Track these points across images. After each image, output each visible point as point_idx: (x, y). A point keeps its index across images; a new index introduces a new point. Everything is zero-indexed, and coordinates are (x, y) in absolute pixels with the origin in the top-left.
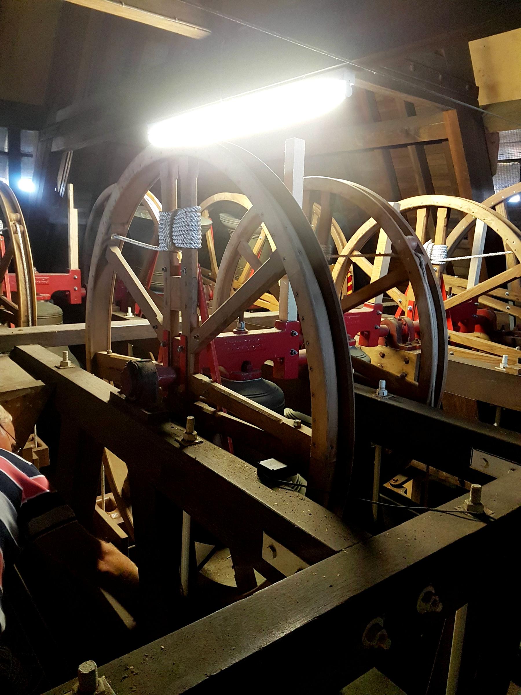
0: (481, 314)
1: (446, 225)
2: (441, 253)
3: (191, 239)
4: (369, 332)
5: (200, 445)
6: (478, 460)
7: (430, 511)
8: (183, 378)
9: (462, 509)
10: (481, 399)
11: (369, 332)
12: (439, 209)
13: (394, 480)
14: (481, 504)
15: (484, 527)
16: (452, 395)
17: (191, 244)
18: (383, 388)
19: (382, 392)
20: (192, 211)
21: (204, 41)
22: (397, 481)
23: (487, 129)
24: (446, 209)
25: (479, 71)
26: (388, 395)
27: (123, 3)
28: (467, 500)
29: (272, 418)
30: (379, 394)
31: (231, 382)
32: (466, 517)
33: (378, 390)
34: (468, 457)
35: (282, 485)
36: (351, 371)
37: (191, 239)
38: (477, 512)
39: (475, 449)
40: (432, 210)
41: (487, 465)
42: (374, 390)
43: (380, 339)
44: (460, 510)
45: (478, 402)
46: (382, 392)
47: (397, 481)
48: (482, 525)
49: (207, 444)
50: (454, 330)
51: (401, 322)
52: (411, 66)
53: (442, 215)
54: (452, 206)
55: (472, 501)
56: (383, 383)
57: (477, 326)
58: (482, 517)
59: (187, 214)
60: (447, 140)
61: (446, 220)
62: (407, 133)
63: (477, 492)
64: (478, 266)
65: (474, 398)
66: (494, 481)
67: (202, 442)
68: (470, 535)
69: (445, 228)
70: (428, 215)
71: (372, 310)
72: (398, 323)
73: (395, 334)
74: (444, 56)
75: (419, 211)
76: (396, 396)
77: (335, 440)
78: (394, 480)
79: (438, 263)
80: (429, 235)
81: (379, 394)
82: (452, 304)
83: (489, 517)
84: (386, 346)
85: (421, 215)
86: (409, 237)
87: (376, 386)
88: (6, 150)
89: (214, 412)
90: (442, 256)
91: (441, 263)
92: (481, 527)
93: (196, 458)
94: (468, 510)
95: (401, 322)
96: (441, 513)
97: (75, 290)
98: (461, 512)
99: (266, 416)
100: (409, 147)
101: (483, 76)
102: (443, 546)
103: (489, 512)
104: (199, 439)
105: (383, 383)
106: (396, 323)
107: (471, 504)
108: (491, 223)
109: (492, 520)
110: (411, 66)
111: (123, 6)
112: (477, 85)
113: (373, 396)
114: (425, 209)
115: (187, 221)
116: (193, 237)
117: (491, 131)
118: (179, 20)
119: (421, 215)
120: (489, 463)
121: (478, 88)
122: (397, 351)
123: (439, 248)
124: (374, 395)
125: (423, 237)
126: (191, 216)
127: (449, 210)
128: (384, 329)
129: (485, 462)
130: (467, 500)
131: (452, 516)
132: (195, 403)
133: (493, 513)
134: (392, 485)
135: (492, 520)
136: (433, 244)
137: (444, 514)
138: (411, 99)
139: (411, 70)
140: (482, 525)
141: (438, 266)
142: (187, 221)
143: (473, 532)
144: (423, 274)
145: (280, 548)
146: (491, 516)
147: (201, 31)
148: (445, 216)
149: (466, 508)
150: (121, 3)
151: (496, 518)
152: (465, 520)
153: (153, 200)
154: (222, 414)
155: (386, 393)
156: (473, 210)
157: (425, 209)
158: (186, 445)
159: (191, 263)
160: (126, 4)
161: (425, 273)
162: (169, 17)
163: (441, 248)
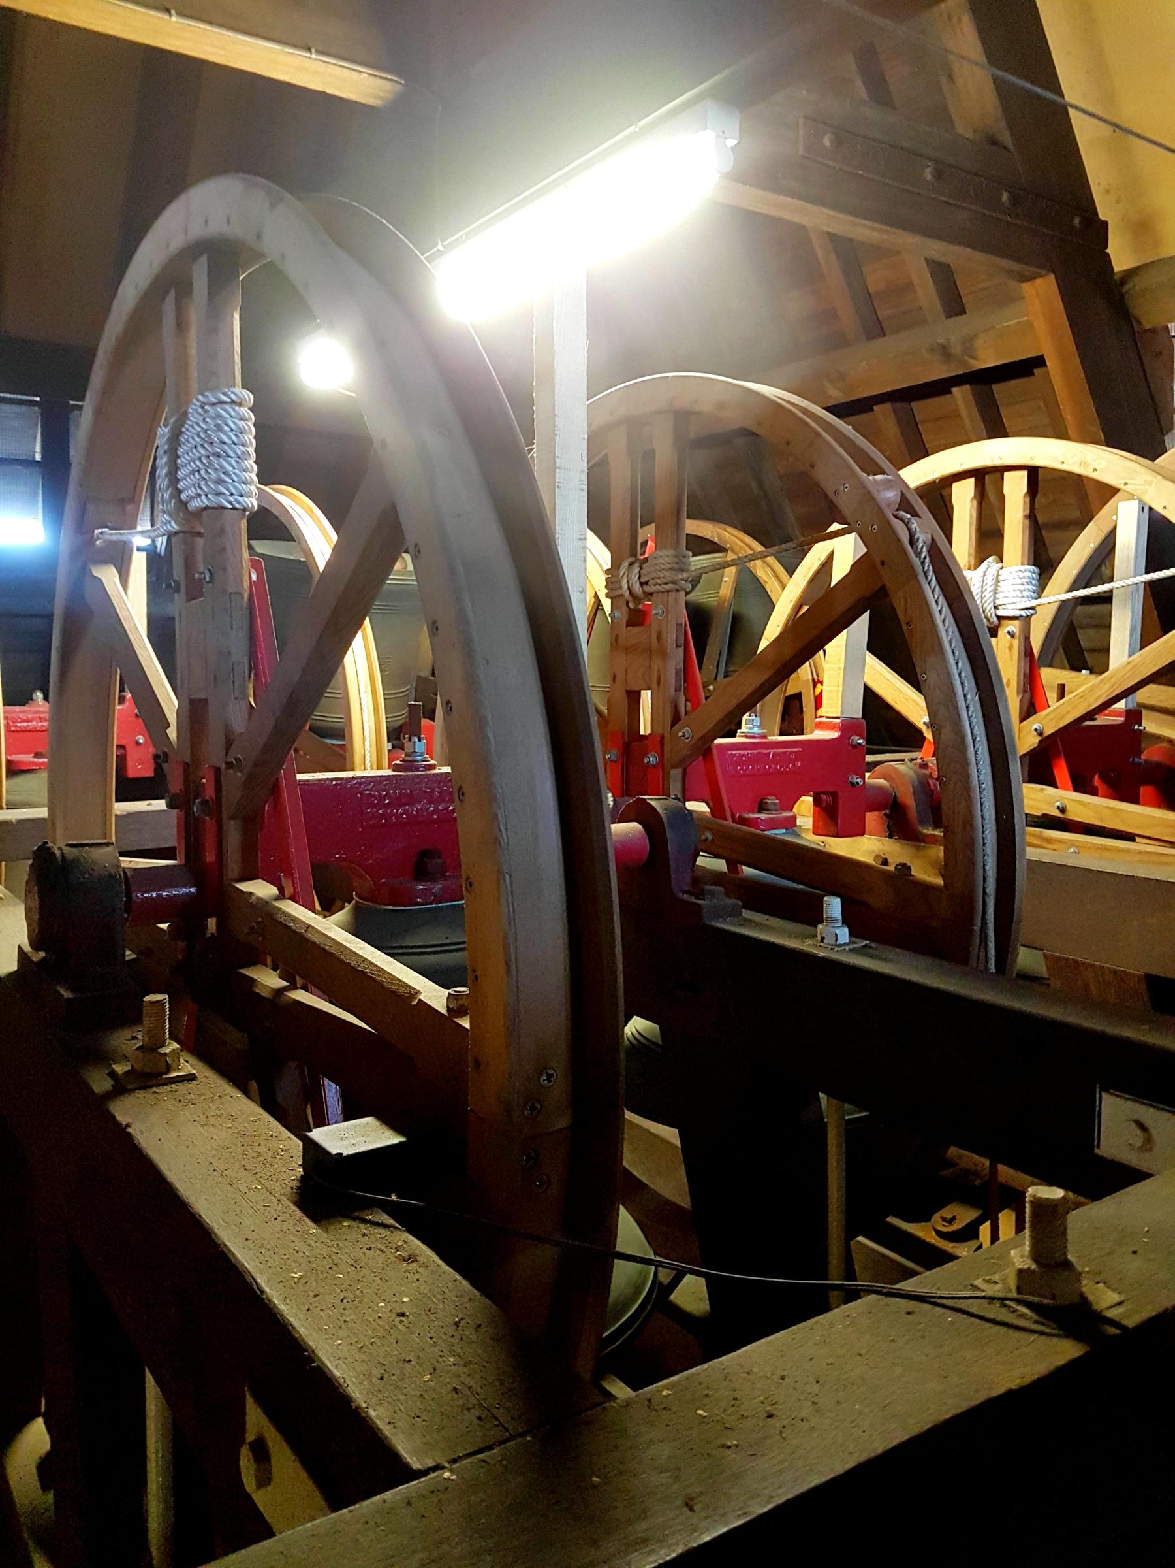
0: (1156, 758)
1: (1028, 512)
2: (1022, 587)
3: (220, 482)
4: (834, 795)
5: (182, 1088)
6: (1118, 1122)
7: (873, 1297)
8: (214, 893)
9: (998, 1287)
10: (1155, 971)
11: (834, 795)
12: (1006, 474)
13: (944, 1219)
14: (1067, 1265)
15: (46, 1423)
16: (1077, 962)
17: (219, 494)
18: (833, 921)
19: (834, 935)
20: (223, 402)
21: (397, 107)
22: (952, 1220)
23: (1139, 323)
24: (1025, 473)
25: (1108, 191)
26: (851, 943)
27: (173, 12)
28: (1012, 1250)
29: (394, 988)
30: (823, 939)
31: (378, 911)
32: (1011, 1318)
33: (820, 926)
34: (1089, 1119)
35: (362, 1209)
36: (600, 800)
37: (220, 482)
38: (1052, 1299)
39: (1107, 1091)
40: (987, 479)
41: (1148, 1142)
42: (809, 929)
43: (872, 818)
44: (990, 1290)
45: (1152, 981)
46: (834, 935)
47: (952, 1220)
48: (1066, 1351)
49: (211, 1081)
50: (1076, 790)
51: (927, 772)
52: (928, 170)
53: (1015, 487)
54: (1038, 462)
55: (1036, 1255)
56: (834, 906)
57: (1145, 791)
58: (1072, 1316)
59: (206, 411)
61: (1028, 500)
62: (945, 352)
63: (1048, 1221)
64: (1133, 630)
65: (1136, 970)
67: (191, 1078)
68: (1010, 1393)
69: (1027, 522)
70: (981, 494)
71: (835, 735)
72: (916, 772)
73: (910, 801)
74: (1011, 147)
75: (956, 487)
76: (873, 945)
77: (563, 1047)
78: (944, 1219)
79: (1017, 613)
80: (989, 540)
81: (823, 939)
82: (1062, 718)
83: (1099, 1318)
84: (890, 836)
85: (963, 496)
86: (879, 477)
87: (812, 916)
88: (38, 457)
89: (280, 992)
90: (1025, 593)
91: (1023, 613)
92: (1061, 1360)
93: (128, 1126)
94: (1019, 1291)
95: (927, 772)
96: (912, 1305)
97: (138, 744)
98: (991, 1299)
99: (381, 985)
100: (955, 390)
101: (1118, 202)
102: (878, 1445)
103: (1105, 1299)
104: (187, 1065)
105: (834, 906)
106: (912, 773)
107: (1028, 1264)
108: (1145, 492)
109: (1113, 1331)
110: (928, 170)
111: (174, 19)
112: (1102, 217)
113: (806, 946)
114: (972, 480)
115: (205, 431)
116: (226, 473)
117: (1147, 326)
118: (318, 52)
119: (963, 496)
120: (1152, 1131)
121: (1105, 224)
122: (918, 848)
123: (1015, 575)
124: (808, 942)
125: (973, 552)
126: (219, 416)
127: (1033, 472)
128: (880, 788)
129: (1139, 1132)
130: (1012, 1250)
131: (951, 1317)
132: (245, 971)
133: (1120, 1303)
134: (940, 1234)
135: (1113, 1331)
136: (1000, 565)
137: (927, 1306)
138: (938, 249)
139: (929, 177)
140: (1066, 1351)
141: (1017, 622)
142: (205, 431)
143: (1028, 1380)
144: (925, 573)
145: (283, 1457)
146: (1110, 1314)
147: (379, 81)
148: (1025, 489)
149: (1012, 1283)
150: (168, 11)
151: (1130, 1323)
152: (1003, 1330)
153: (311, 513)
154: (301, 996)
155: (844, 934)
156: (1095, 465)
157: (972, 480)
158: (130, 1087)
159: (224, 550)
160: (179, 14)
161: (931, 573)
162: (295, 46)
163: (1021, 575)
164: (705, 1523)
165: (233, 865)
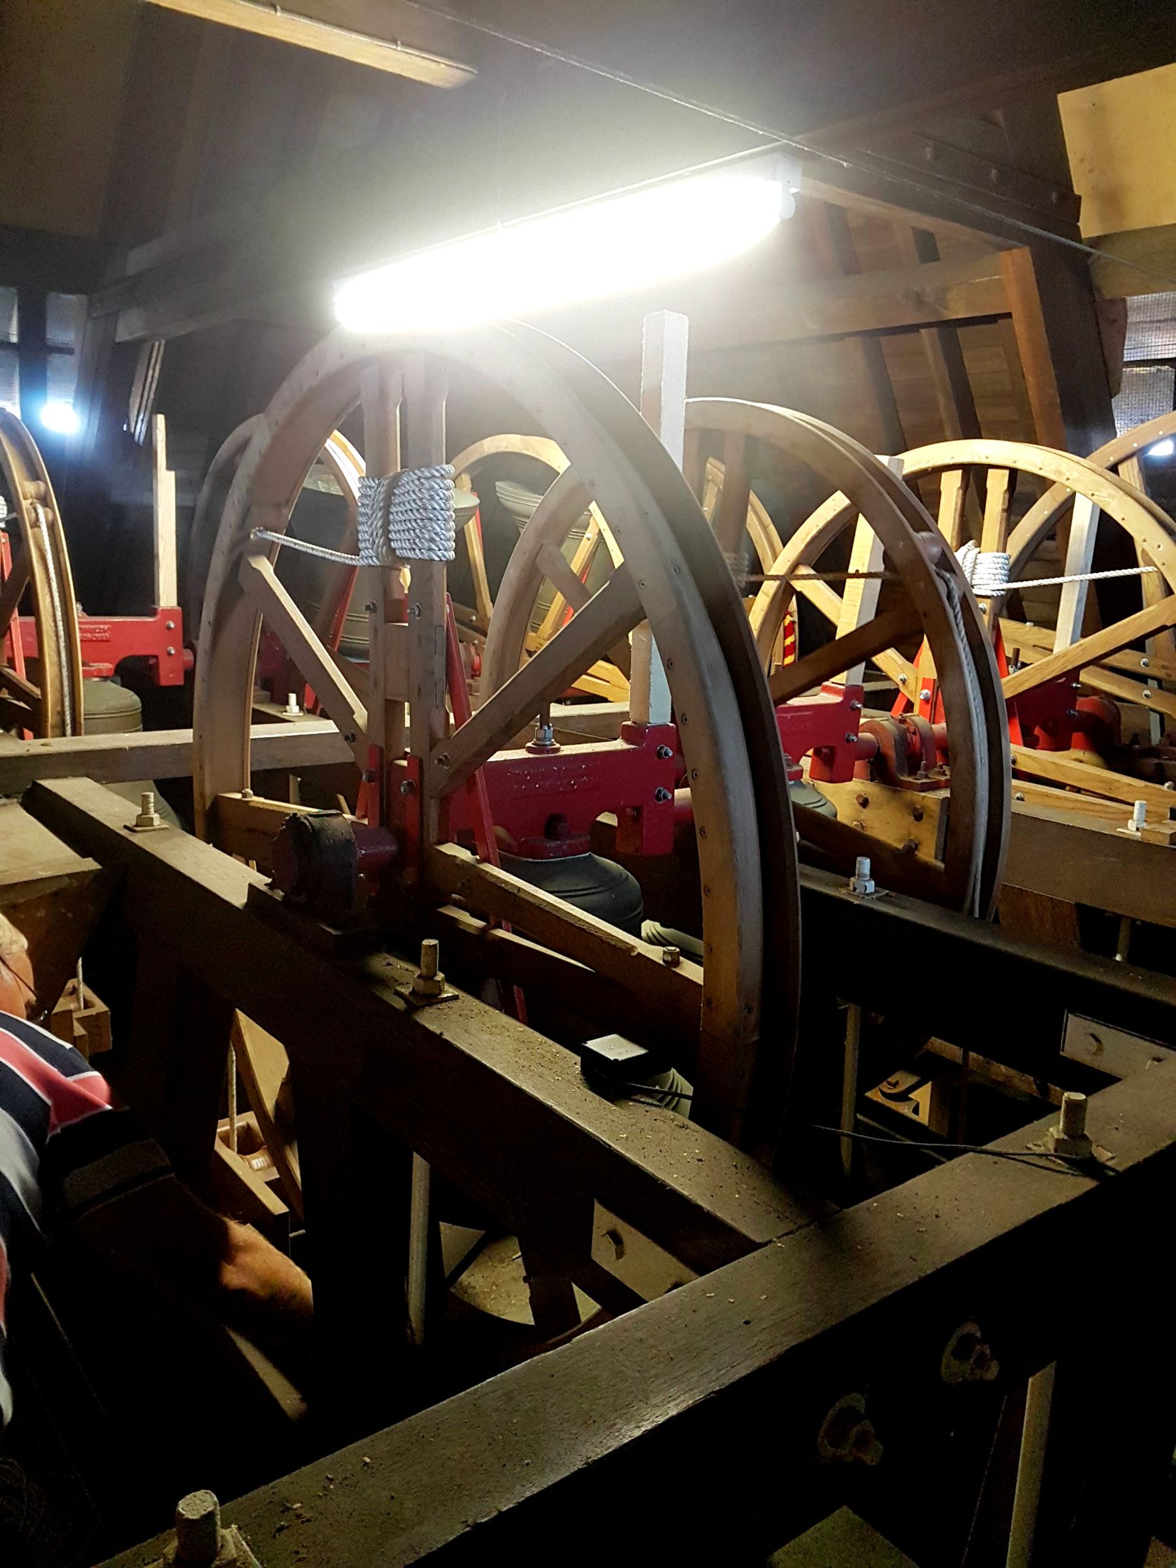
0: (1087, 709)
1: (1006, 507)
2: (995, 572)
3: (432, 540)
4: (832, 749)
5: (452, 1004)
6: (1079, 1037)
7: (971, 1154)
8: (414, 852)
9: (1042, 1148)
10: (1085, 901)
11: (832, 749)
12: (990, 471)
13: (889, 1083)
14: (1085, 1137)
15: (1092, 1189)
16: (1021, 890)
17: (430, 549)
18: (865, 876)
19: (863, 885)
20: (434, 476)
21: (461, 92)
22: (895, 1085)
23: (1099, 291)
24: (1007, 472)
25: (1082, 161)
26: (876, 891)
27: (278, 8)
28: (1054, 1129)
29: (613, 943)
30: (855, 889)
31: (521, 861)
32: (1052, 1166)
33: (852, 879)
34: (1057, 1032)
35: (636, 1094)
37: (432, 540)
38: (1076, 1154)
39: (1072, 1013)
40: (975, 475)
41: (1100, 1048)
42: (844, 879)
43: (859, 765)
44: (1038, 1150)
45: (1079, 906)
46: (863, 885)
47: (895, 1085)
48: (1088, 1184)
49: (468, 1001)
50: (1026, 745)
51: (904, 726)
52: (928, 149)
53: (997, 484)
54: (1020, 465)
55: (1066, 1131)
56: (864, 865)
57: (1077, 736)
58: (1088, 1166)
59: (422, 484)
60: (1009, 315)
61: (1007, 496)
62: (919, 300)
63: (1076, 1110)
64: (1079, 601)
65: (1069, 897)
66: (1114, 1086)
67: (455, 998)
68: (1060, 1206)
69: (1005, 514)
70: (965, 486)
71: (839, 699)
72: (897, 728)
73: (891, 753)
74: (1003, 125)
75: (945, 476)
76: (893, 894)
77: (757, 992)
78: (889, 1083)
79: (989, 593)
80: (969, 530)
81: (855, 889)
82: (1020, 685)
83: (1103, 1166)
84: (872, 780)
85: (951, 485)
86: (924, 534)
87: (849, 870)
88: (14, 339)
89: (484, 930)
90: (998, 577)
91: (994, 594)
92: (1085, 1189)
93: (441, 1034)
94: (1056, 1150)
95: (904, 726)
96: (996, 1158)
97: (169, 654)
98: (1040, 1155)
99: (600, 938)
100: (923, 331)
101: (1091, 171)
103: (1103, 1155)
104: (449, 991)
105: (864, 865)
106: (893, 728)
107: (1063, 1136)
108: (1109, 503)
109: (1112, 1174)
110: (928, 149)
111: (279, 14)
112: (1076, 192)
113: (842, 894)
114: (960, 472)
115: (421, 499)
116: (436, 534)
117: (1108, 296)
118: (403, 44)
119: (951, 485)
120: (1105, 1044)
121: (1078, 199)
122: (895, 791)
123: (991, 560)
124: (844, 891)
125: (955, 535)
126: (432, 488)
127: (1014, 473)
128: (867, 742)
129: (1095, 1043)
130: (1054, 1129)
131: (1020, 1165)
132: (441, 910)
133: (1113, 1158)
134: (884, 1094)
135: (1112, 1174)
136: (978, 550)
137: (1003, 1159)
138: (927, 222)
139: (929, 157)
140: (1088, 1184)
141: (989, 601)
142: (421, 499)
143: (1069, 1199)
144: (956, 617)
145: (632, 1237)
146: (1109, 1163)
147: (455, 70)
148: (1005, 486)
149: (1051, 1147)
150: (274, 7)
151: (1120, 1169)
152: (1050, 1172)
153: (345, 450)
154: (501, 933)
155: (871, 886)
156: (1068, 475)
157: (960, 472)
158: (420, 1004)
159: (432, 593)
160: (284, 9)
161: (960, 615)
162: (383, 39)
163: (996, 560)
164: (642, 1316)
165: (433, 835)
